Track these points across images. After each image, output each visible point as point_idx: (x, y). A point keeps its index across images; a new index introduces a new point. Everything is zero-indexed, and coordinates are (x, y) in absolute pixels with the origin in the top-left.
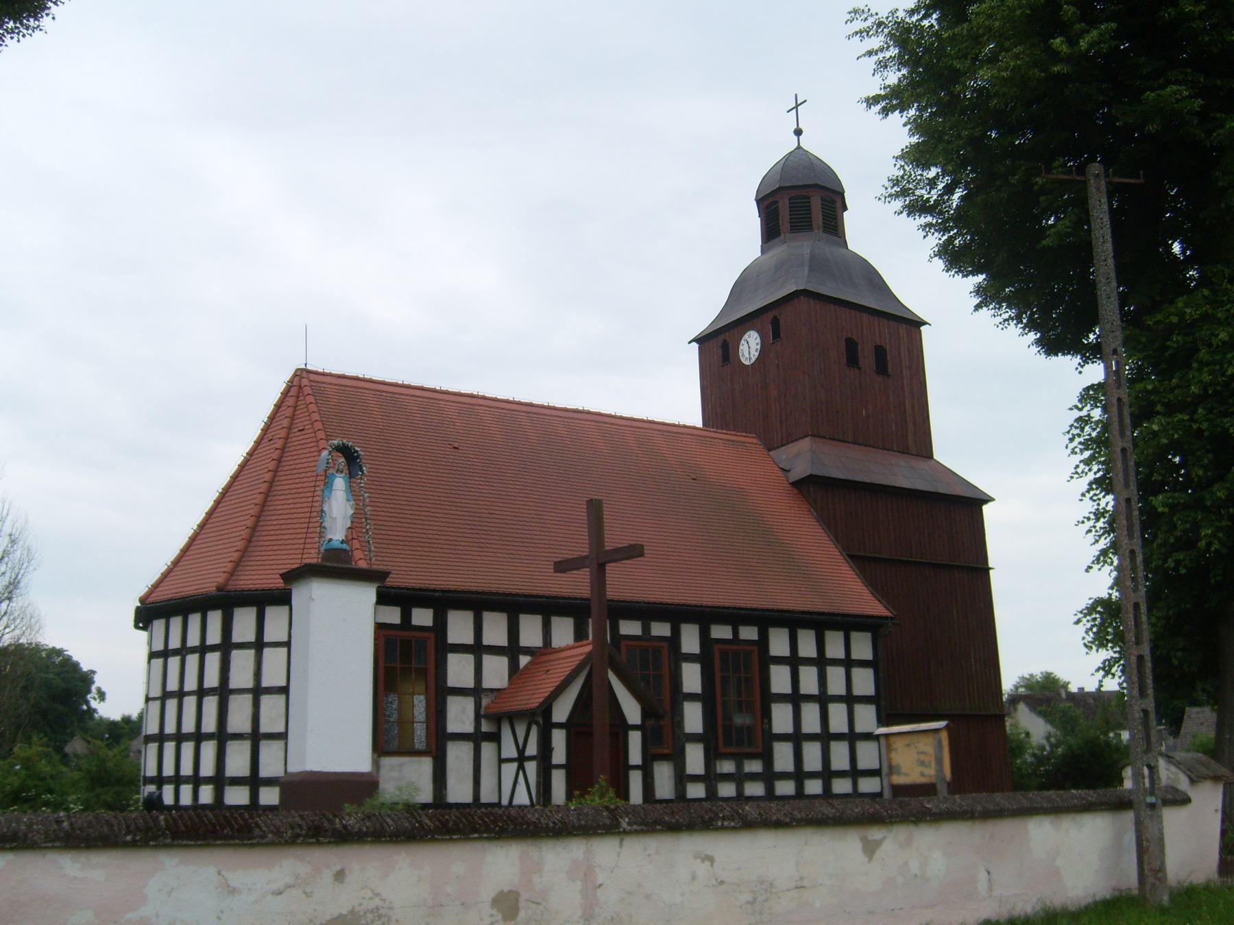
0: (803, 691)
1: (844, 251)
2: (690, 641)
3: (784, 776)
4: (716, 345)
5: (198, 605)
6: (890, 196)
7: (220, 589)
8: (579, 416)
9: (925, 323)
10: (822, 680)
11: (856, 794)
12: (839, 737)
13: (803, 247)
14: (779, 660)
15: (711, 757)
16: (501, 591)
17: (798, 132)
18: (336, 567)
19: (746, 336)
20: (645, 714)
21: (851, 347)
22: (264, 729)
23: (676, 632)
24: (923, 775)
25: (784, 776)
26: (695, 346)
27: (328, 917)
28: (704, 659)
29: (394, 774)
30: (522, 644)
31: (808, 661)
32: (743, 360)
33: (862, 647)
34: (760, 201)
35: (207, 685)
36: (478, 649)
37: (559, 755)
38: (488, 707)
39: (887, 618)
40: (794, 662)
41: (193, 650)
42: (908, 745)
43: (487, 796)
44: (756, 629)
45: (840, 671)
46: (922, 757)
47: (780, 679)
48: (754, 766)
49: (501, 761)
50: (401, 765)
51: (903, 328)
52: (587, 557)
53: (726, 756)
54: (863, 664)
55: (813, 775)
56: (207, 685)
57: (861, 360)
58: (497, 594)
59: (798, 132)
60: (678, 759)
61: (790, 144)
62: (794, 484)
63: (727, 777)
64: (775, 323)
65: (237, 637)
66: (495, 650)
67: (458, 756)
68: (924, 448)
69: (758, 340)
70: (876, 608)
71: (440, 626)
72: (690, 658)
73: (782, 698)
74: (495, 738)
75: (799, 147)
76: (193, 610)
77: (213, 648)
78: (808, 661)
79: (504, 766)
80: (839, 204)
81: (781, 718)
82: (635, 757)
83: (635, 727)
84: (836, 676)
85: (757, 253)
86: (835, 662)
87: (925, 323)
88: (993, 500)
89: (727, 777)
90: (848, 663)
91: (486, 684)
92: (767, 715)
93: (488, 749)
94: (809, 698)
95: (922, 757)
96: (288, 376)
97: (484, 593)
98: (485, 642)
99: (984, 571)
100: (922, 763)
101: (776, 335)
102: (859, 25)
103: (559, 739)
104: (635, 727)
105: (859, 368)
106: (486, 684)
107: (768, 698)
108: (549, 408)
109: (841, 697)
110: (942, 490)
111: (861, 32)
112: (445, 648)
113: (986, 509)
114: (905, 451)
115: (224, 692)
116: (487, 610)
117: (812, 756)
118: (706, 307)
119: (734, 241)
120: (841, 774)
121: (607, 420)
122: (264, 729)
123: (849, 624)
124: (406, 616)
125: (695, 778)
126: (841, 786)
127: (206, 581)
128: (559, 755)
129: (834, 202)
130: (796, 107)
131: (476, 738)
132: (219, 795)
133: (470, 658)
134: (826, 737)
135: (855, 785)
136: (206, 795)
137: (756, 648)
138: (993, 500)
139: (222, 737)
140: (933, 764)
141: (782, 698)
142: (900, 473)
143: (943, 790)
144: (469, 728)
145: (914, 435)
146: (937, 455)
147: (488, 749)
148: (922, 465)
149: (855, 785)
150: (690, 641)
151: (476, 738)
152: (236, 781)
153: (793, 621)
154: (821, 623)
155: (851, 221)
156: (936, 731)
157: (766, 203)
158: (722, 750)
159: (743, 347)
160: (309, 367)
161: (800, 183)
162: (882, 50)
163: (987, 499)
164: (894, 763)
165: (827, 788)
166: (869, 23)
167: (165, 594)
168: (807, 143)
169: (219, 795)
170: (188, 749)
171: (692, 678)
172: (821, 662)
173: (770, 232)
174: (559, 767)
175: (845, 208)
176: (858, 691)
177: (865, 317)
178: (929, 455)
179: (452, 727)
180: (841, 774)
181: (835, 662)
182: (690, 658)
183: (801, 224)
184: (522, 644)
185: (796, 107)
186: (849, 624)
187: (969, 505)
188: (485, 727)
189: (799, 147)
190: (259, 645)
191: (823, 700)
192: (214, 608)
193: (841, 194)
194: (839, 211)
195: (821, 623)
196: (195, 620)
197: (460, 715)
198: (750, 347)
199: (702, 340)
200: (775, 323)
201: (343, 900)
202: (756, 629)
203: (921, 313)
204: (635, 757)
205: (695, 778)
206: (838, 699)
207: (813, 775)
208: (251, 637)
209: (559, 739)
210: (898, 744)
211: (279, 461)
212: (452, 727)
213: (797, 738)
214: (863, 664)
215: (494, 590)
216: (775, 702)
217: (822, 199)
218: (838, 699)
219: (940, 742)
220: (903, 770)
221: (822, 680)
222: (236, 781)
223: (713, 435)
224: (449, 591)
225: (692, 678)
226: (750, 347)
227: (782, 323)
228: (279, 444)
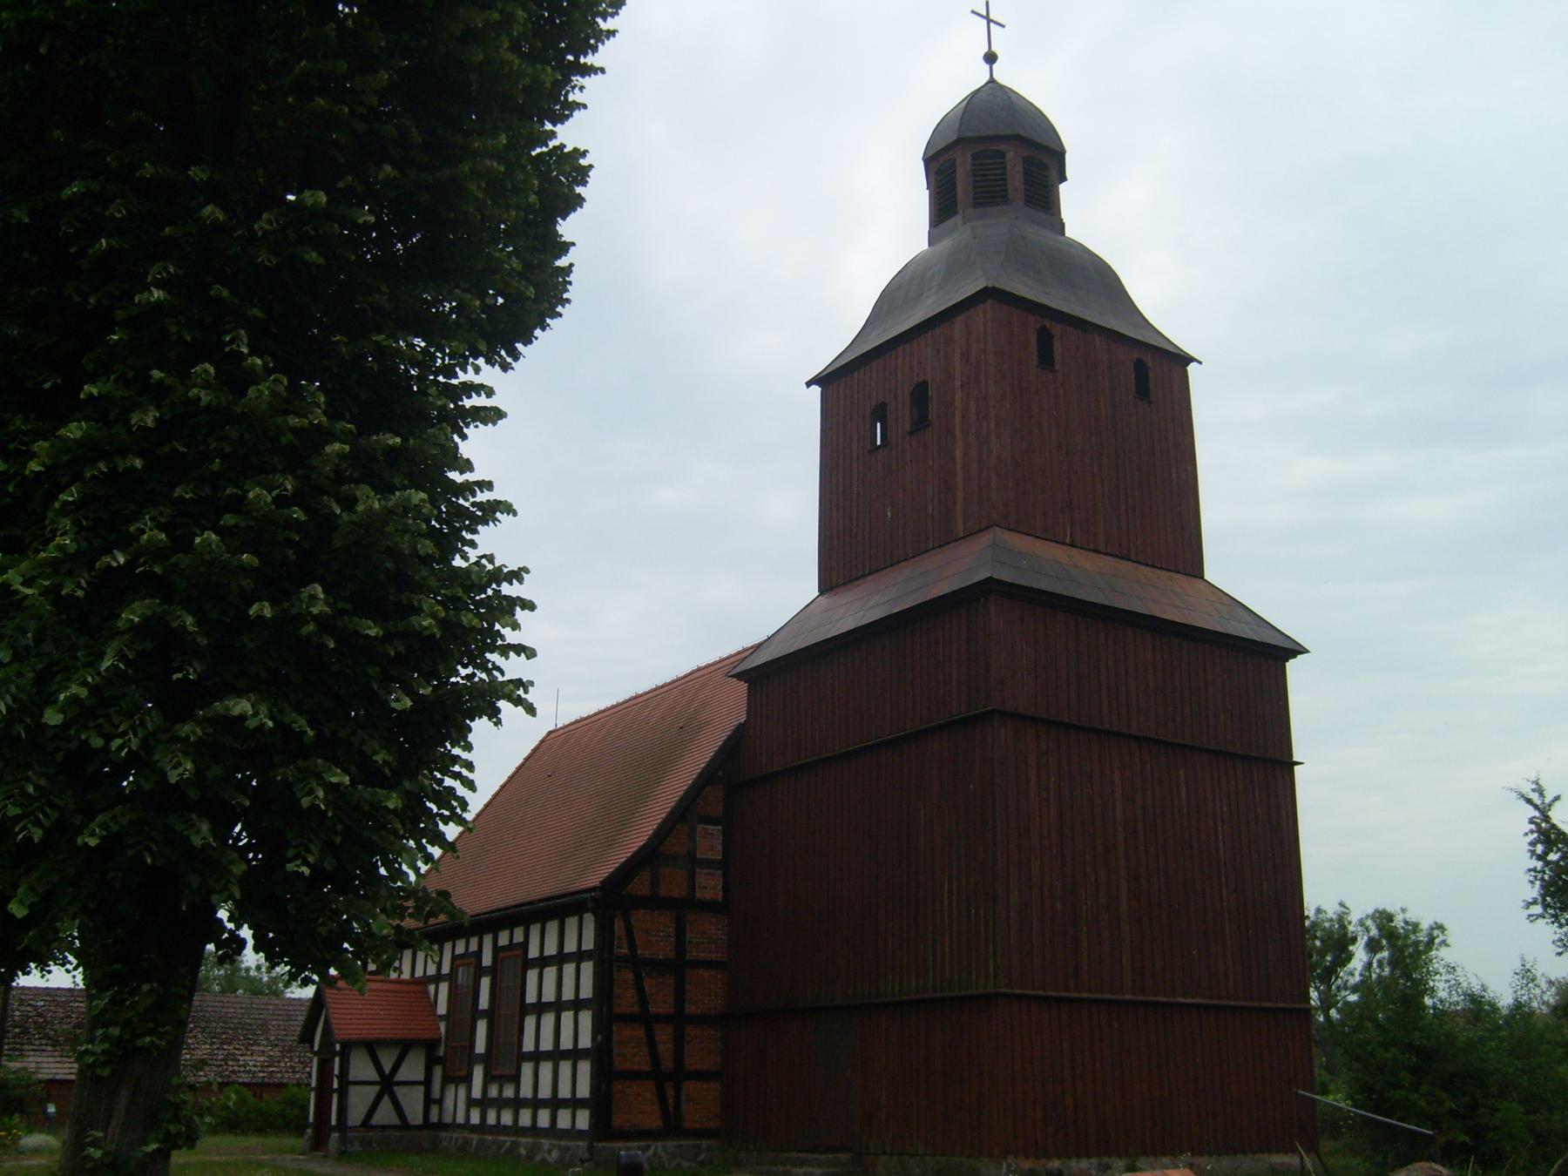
13: (998, 225)
17: (991, 58)
26: (816, 390)
44: (587, 1095)
59: (991, 58)
75: (992, 81)
80: (1054, 173)
85: (923, 245)
88: (1306, 651)
99: (1286, 765)
129: (1045, 167)
130: (989, 21)
138: (1306, 651)
142: (1158, 596)
145: (1175, 535)
146: (1210, 574)
161: (992, 133)
163: (1295, 650)
168: (1001, 78)
170: (546, 1069)
173: (943, 208)
175: (1063, 178)
183: (990, 194)
185: (989, 21)
187: (1267, 656)
189: (992, 81)
202: (587, 1095)
217: (1025, 160)
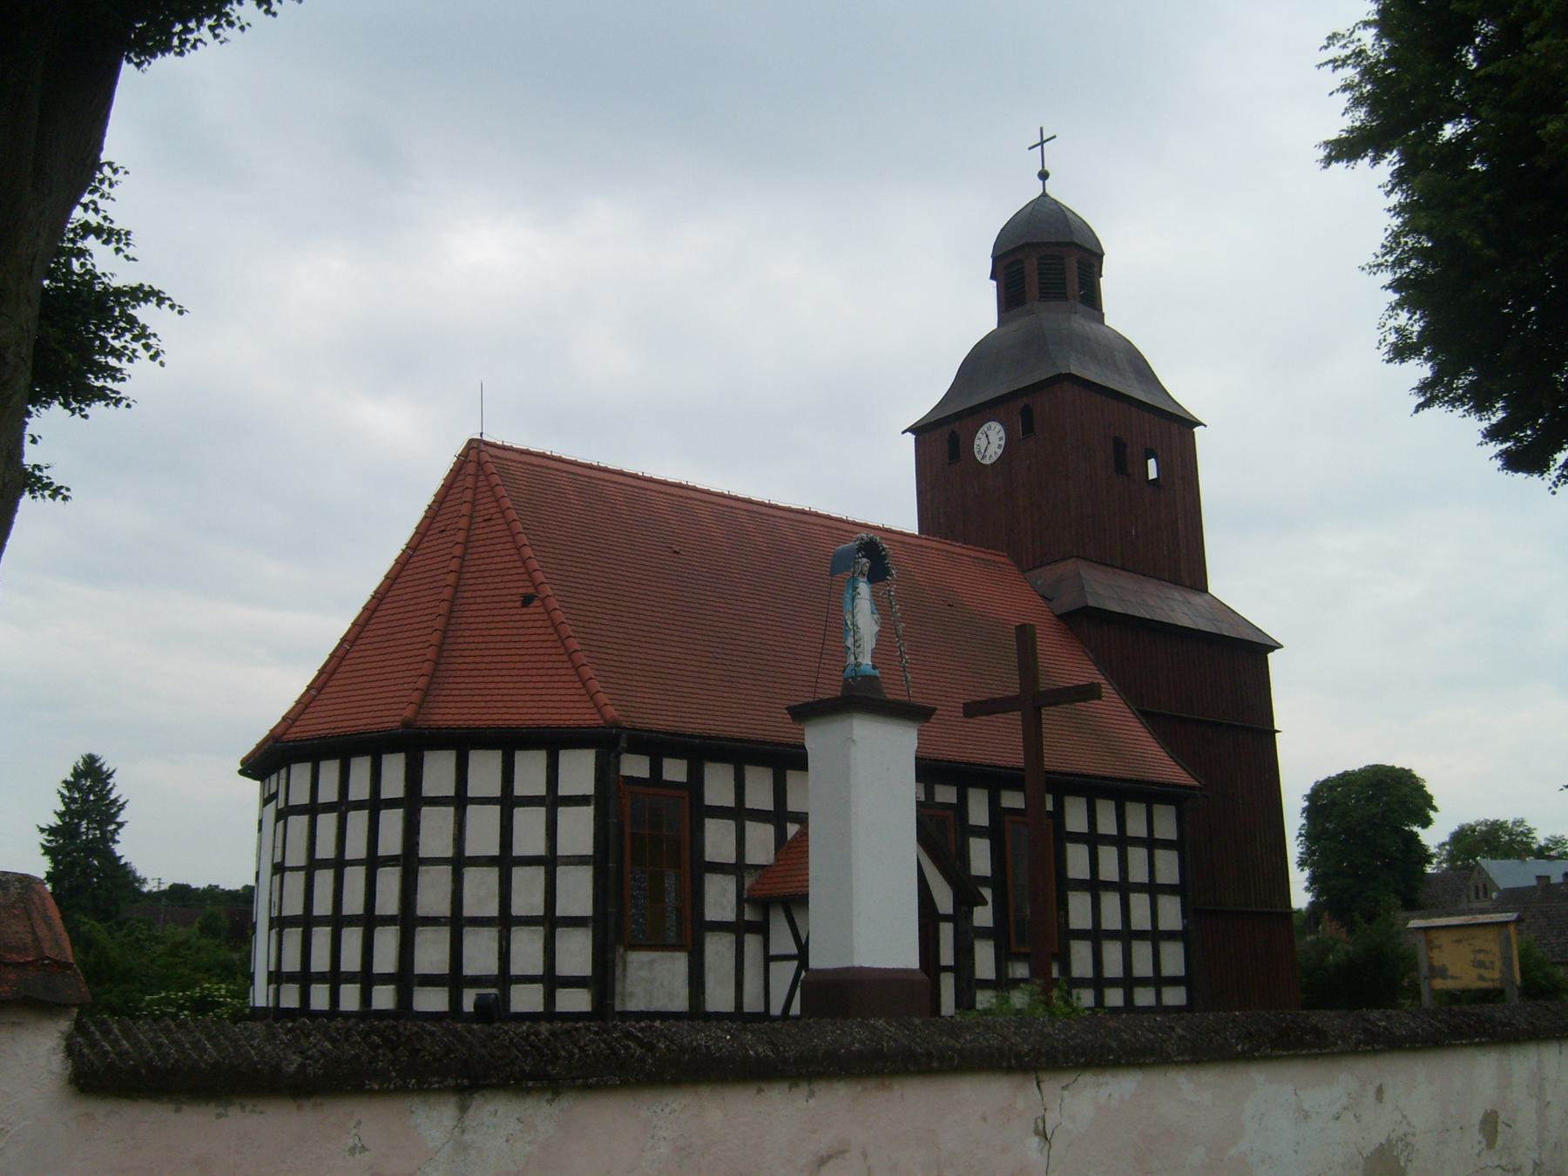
1: (1094, 326)
4: (940, 439)
5: (342, 748)
6: (1379, 265)
7: (406, 725)
8: (805, 518)
9: (1199, 424)
11: (550, 1014)
12: (1112, 935)
16: (769, 739)
17: (1044, 175)
18: (861, 698)
19: (985, 428)
22: (468, 911)
24: (1481, 978)
26: (911, 437)
27: (1372, 1148)
28: (994, 833)
29: (644, 973)
30: (790, 809)
33: (1166, 827)
34: (997, 258)
35: (383, 851)
36: (739, 814)
38: (751, 889)
39: (1194, 788)
41: (328, 808)
42: (1459, 941)
43: (752, 1003)
46: (1481, 957)
49: (768, 959)
50: (652, 962)
52: (1016, 697)
53: (1020, 957)
54: (1167, 844)
56: (383, 851)
58: (764, 743)
61: (1033, 191)
62: (1060, 617)
64: (1027, 414)
65: (428, 790)
66: (759, 816)
67: (718, 950)
68: (1198, 581)
69: (1002, 434)
70: (1180, 776)
71: (696, 782)
72: (979, 832)
74: (762, 929)
75: (1044, 195)
76: (360, 751)
77: (392, 804)
79: (773, 966)
83: (946, 918)
85: (994, 326)
87: (1199, 424)
90: (1151, 843)
91: (750, 859)
92: (1063, 906)
93: (752, 943)
95: (1481, 957)
96: (459, 446)
97: (749, 741)
99: (1272, 733)
100: (1481, 964)
101: (1028, 428)
102: (1336, 52)
104: (946, 918)
105: (1128, 475)
106: (750, 859)
108: (770, 506)
109: (1143, 885)
110: (1227, 631)
111: (1334, 61)
113: (1272, 657)
114: (1177, 582)
115: (410, 862)
116: (751, 763)
118: (928, 390)
119: (965, 311)
120: (1144, 982)
121: (839, 525)
122: (468, 911)
123: (1151, 793)
124: (656, 768)
126: (1144, 997)
127: (387, 709)
130: (1042, 143)
131: (738, 929)
132: (404, 998)
133: (730, 825)
135: (1158, 995)
136: (350, 998)
139: (408, 921)
140: (1498, 964)
142: (1178, 610)
143: (1513, 997)
144: (730, 916)
145: (1184, 562)
147: (752, 943)
148: (1197, 599)
149: (1158, 995)
150: (979, 814)
151: (738, 929)
152: (430, 980)
153: (1092, 788)
154: (1123, 791)
156: (1505, 924)
158: (1015, 949)
159: (980, 442)
160: (485, 438)
162: (1359, 85)
163: (1275, 646)
164: (1436, 963)
165: (1129, 998)
166: (1348, 52)
167: (314, 727)
168: (1055, 190)
169: (404, 998)
176: (1162, 878)
178: (1206, 591)
181: (1137, 841)
182: (979, 832)
183: (1054, 290)
184: (790, 809)
185: (1042, 143)
186: (1151, 793)
188: (749, 915)
189: (1044, 195)
190: (460, 801)
192: (393, 750)
193: (1099, 256)
195: (1123, 791)
196: (361, 769)
197: (720, 899)
198: (990, 442)
200: (1027, 414)
201: (1377, 1128)
203: (1195, 411)
208: (540, 789)
210: (1444, 939)
211: (462, 558)
212: (711, 914)
213: (1096, 935)
214: (1167, 844)
215: (761, 738)
218: (1140, 888)
219: (1508, 938)
220: (1450, 973)
222: (430, 980)
223: (972, 554)
224: (710, 738)
226: (990, 442)
228: (461, 537)
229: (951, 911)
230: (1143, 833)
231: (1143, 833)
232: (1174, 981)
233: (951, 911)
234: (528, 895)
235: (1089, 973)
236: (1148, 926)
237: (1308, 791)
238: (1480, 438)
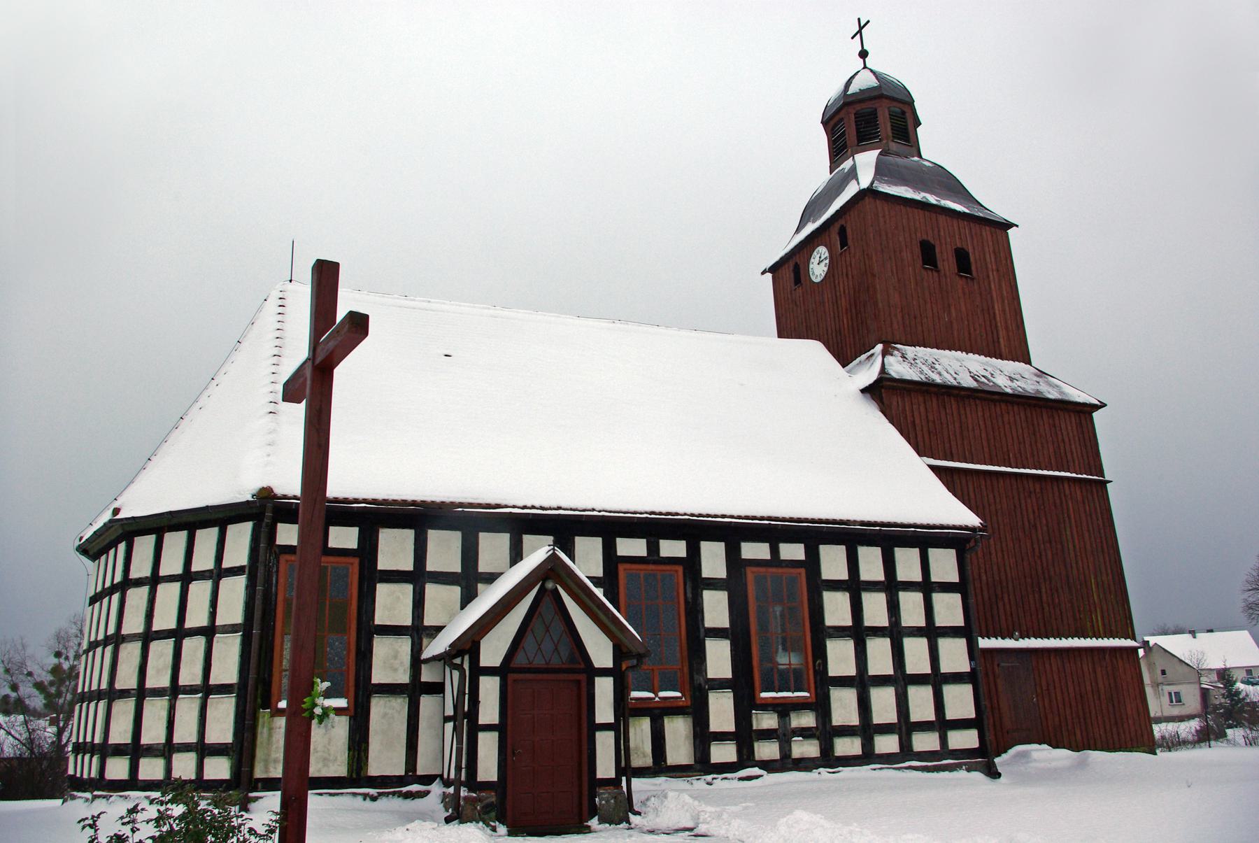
0: (868, 623)
2: (713, 559)
3: (846, 731)
10: (894, 608)
12: (919, 680)
14: (835, 585)
15: (745, 708)
17: (863, 54)
20: (620, 653)
21: (928, 254)
23: (694, 552)
25: (846, 731)
26: (769, 276)
31: (873, 586)
32: (813, 278)
33: (945, 565)
34: (825, 123)
37: (489, 712)
40: (854, 587)
45: (918, 597)
47: (837, 609)
48: (807, 720)
51: (986, 231)
54: (946, 587)
55: (886, 729)
57: (940, 264)
59: (863, 54)
60: (699, 714)
63: (767, 735)
64: (843, 233)
72: (713, 584)
73: (840, 632)
78: (873, 586)
80: (910, 122)
81: (840, 657)
82: (604, 712)
83: (604, 672)
84: (912, 609)
86: (909, 586)
89: (767, 735)
92: (820, 654)
94: (877, 632)
98: (430, 567)
101: (844, 243)
103: (489, 688)
104: (604, 672)
105: (938, 271)
107: (820, 633)
109: (919, 629)
112: (371, 575)
117: (884, 704)
120: (924, 726)
125: (722, 737)
128: (489, 712)
130: (861, 28)
134: (901, 680)
137: (803, 571)
141: (840, 632)
142: (1004, 375)
149: (944, 740)
150: (713, 559)
154: (889, 537)
155: (923, 134)
157: (832, 123)
169: (219, 750)
171: (716, 608)
172: (891, 586)
174: (488, 728)
175: (918, 123)
177: (942, 219)
179: (833, 671)
180: (924, 726)
185: (861, 28)
186: (924, 538)
191: (895, 633)
193: (909, 102)
194: (910, 128)
197: (389, 661)
198: (818, 268)
199: (774, 269)
200: (843, 233)
204: (604, 712)
205: (722, 737)
206: (916, 632)
207: (886, 729)
209: (489, 688)
212: (833, 671)
214: (946, 587)
216: (831, 636)
221: (894, 608)
225: (716, 608)
226: (818, 268)
227: (849, 230)
229: (610, 664)
230: (917, 576)
231: (917, 576)
232: (219, 750)
233: (610, 664)
234: (880, 657)
235: (855, 720)
236: (926, 669)
237: (254, 492)
238: (895, 62)
